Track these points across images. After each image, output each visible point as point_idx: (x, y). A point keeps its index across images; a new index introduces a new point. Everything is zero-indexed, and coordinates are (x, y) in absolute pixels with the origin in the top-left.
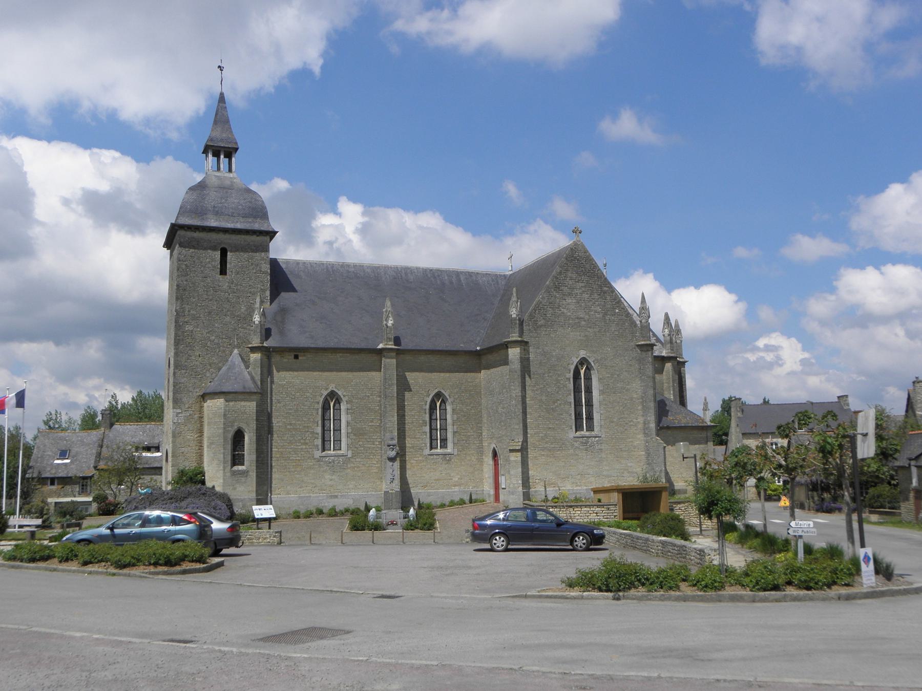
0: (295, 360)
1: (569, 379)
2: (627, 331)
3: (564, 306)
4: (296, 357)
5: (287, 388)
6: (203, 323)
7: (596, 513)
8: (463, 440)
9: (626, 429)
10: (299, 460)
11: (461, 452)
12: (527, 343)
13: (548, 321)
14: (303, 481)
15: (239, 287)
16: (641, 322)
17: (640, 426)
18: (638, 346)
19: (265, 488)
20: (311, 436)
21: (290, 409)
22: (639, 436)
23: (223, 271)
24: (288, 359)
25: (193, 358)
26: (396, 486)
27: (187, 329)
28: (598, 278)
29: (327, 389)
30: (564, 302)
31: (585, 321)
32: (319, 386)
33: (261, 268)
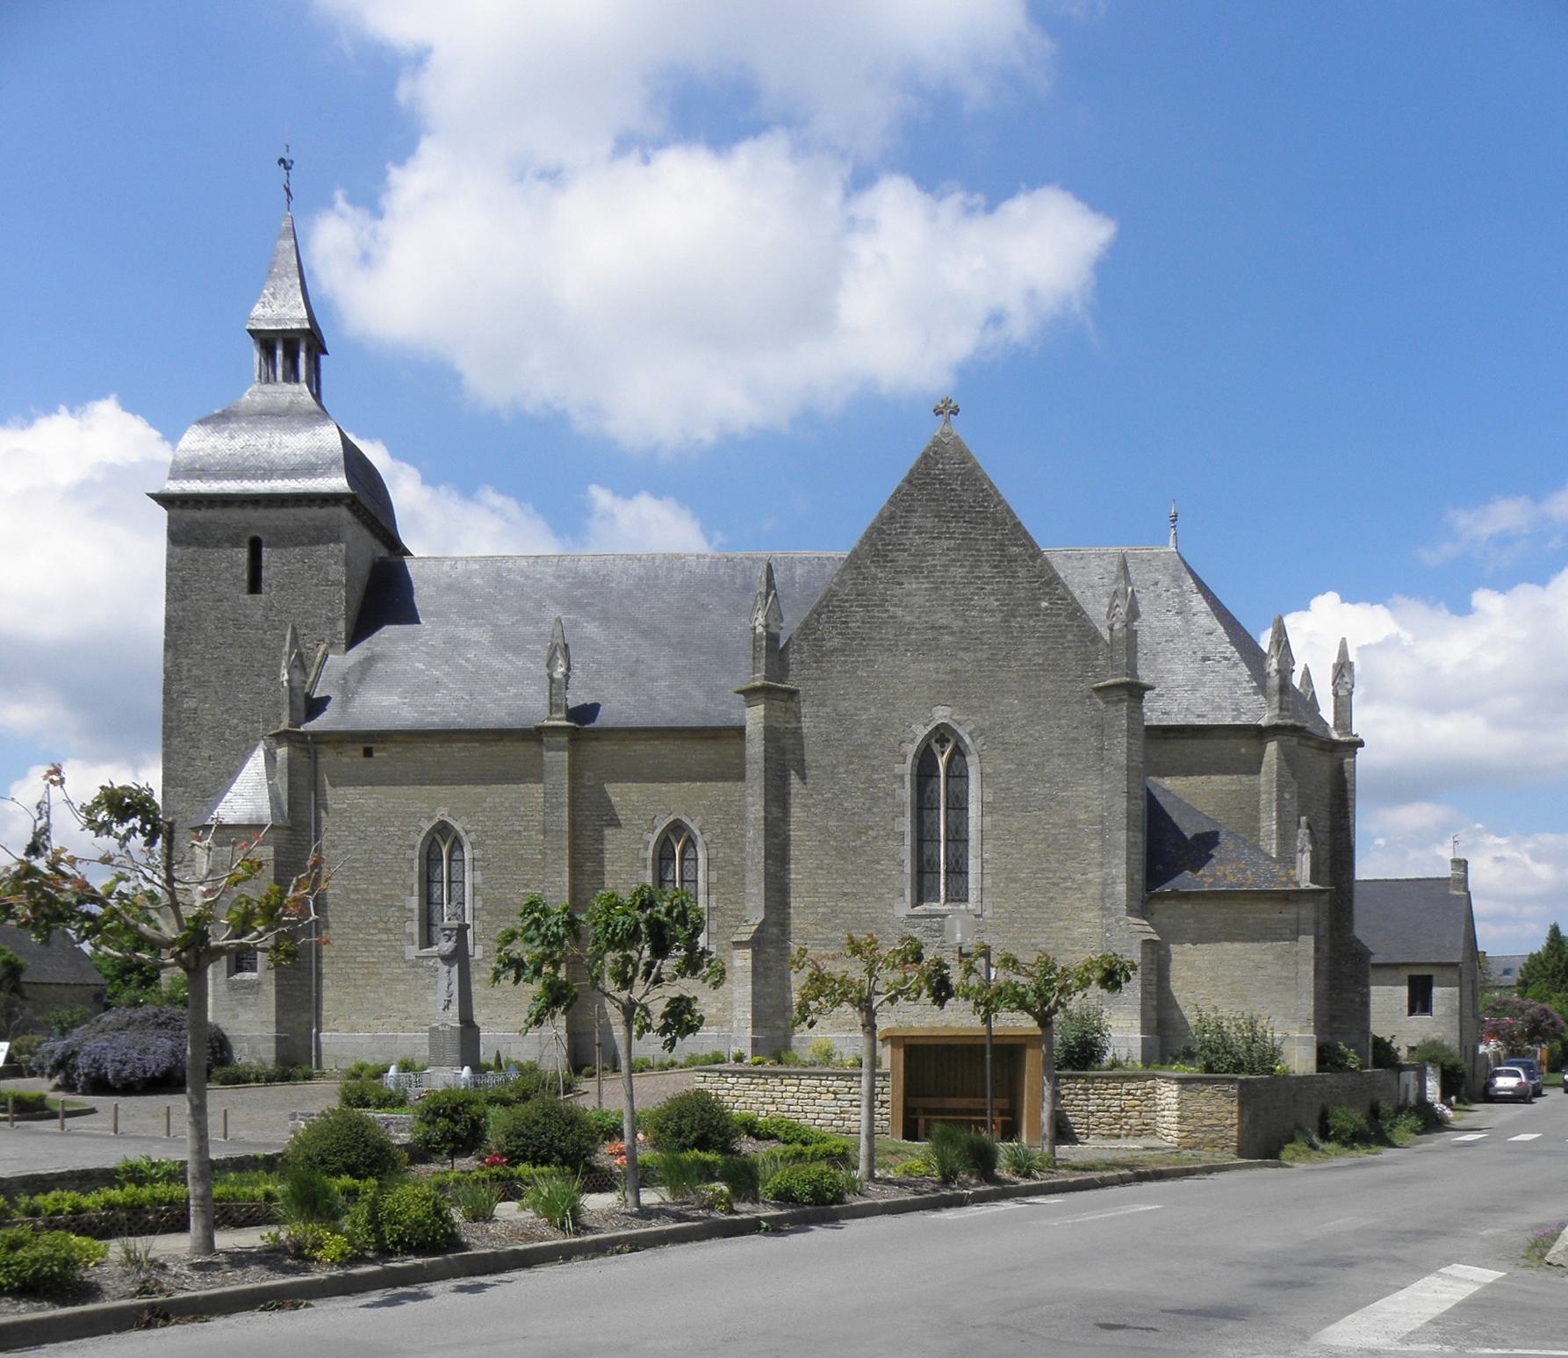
0: (366, 759)
1: (902, 778)
2: (1070, 655)
3: (896, 600)
4: (368, 753)
5: (350, 817)
6: (216, 693)
7: (835, 1093)
8: (731, 926)
9: (1051, 898)
10: (373, 963)
11: (724, 951)
12: (793, 693)
13: (852, 639)
14: (382, 1006)
15: (284, 616)
16: (1111, 629)
17: (1093, 891)
18: (1098, 690)
19: (305, 1017)
20: (397, 914)
21: (356, 860)
22: (1089, 916)
23: (255, 585)
24: (352, 757)
25: (198, 763)
26: (453, 1018)
27: (185, 706)
28: (995, 524)
29: (430, 818)
30: (898, 591)
31: (952, 634)
32: (415, 812)
33: (327, 573)
